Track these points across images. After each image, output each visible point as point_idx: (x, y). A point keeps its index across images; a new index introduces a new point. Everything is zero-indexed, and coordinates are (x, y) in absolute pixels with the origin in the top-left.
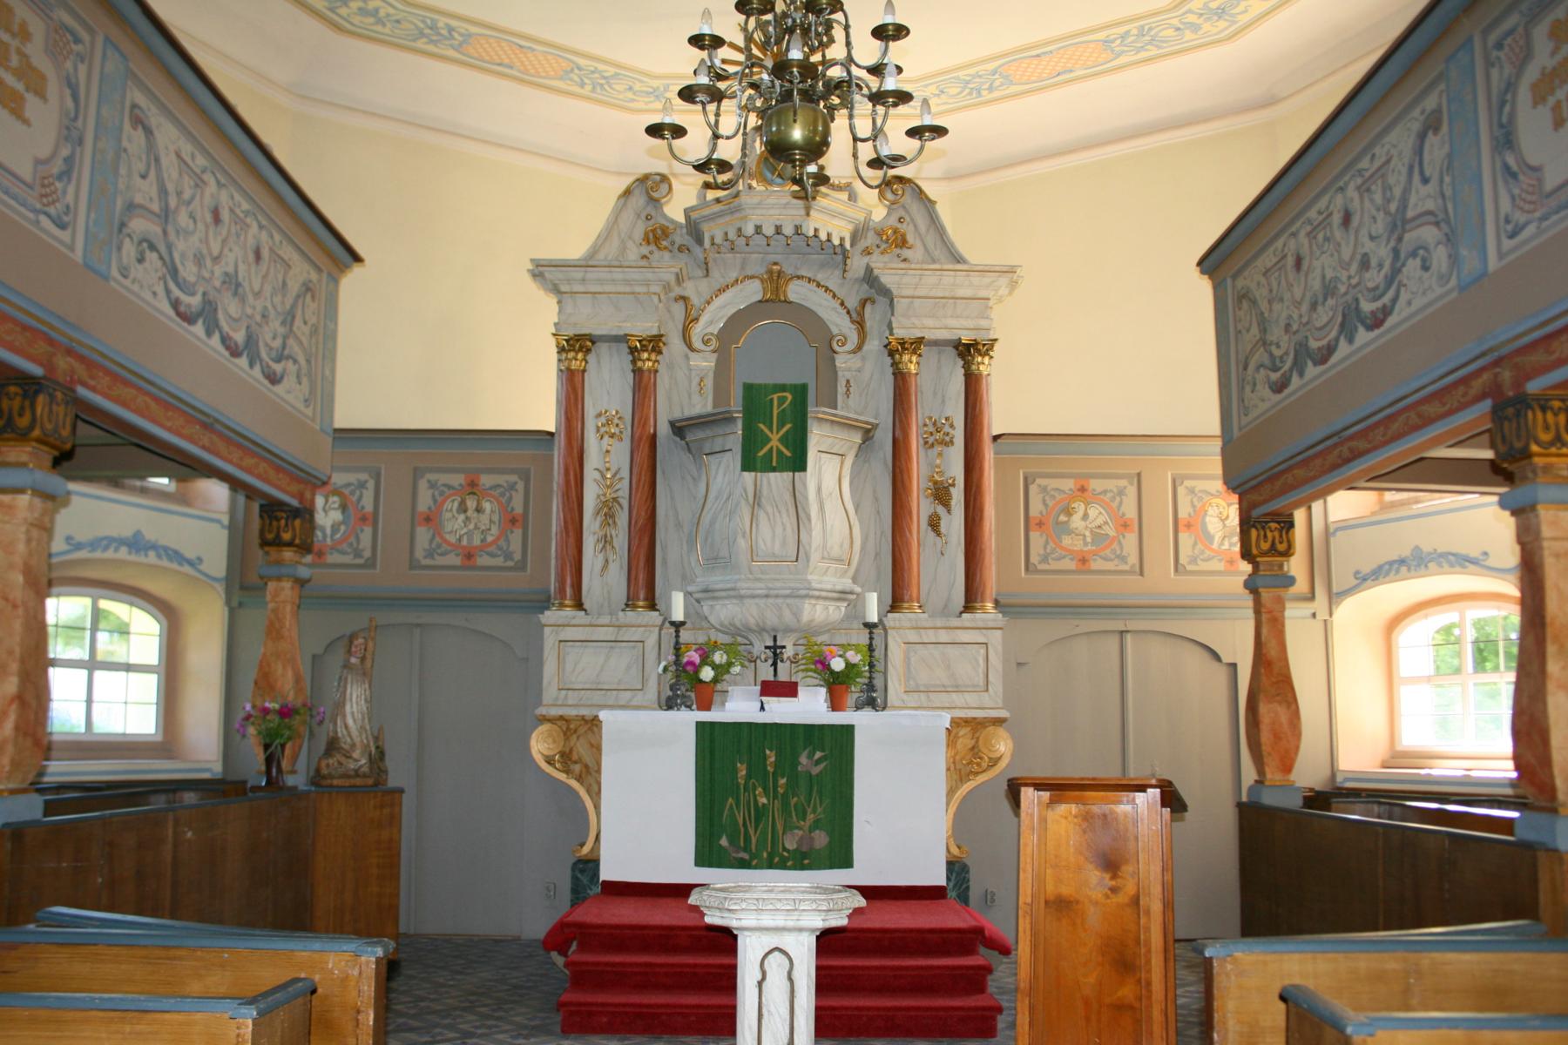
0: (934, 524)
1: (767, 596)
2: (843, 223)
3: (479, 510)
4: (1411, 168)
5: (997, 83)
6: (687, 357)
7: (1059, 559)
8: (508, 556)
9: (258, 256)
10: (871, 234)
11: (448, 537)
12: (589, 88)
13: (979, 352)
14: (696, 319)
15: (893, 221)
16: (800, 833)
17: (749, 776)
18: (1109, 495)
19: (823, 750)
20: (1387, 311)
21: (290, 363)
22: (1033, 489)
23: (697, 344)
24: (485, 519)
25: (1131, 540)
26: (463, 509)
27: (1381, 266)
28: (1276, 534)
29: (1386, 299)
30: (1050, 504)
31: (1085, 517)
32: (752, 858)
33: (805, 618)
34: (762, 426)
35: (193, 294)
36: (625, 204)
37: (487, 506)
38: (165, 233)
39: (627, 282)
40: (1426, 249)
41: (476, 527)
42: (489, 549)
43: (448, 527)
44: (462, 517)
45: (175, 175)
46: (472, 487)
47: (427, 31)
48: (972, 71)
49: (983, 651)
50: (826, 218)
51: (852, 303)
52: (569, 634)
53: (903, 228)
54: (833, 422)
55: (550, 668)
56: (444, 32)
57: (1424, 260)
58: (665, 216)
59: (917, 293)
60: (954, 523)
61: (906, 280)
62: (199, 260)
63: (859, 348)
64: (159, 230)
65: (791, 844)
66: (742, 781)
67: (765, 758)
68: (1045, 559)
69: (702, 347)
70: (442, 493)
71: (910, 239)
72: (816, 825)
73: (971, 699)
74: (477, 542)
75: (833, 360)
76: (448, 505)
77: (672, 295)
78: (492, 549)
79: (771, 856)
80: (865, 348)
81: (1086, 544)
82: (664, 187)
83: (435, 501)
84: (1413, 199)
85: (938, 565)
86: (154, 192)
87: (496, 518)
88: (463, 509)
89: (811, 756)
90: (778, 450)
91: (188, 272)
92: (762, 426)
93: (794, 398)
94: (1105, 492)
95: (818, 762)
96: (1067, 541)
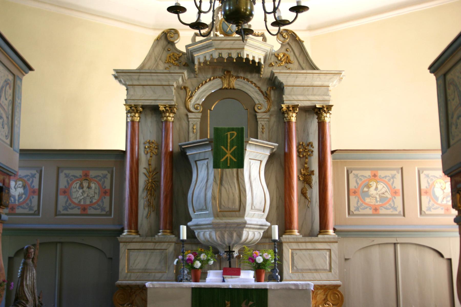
2: (260, 52)
3: (89, 187)
8: (103, 209)
11: (74, 200)
18: (387, 178)
19: (253, 301)
24: (92, 192)
26: (81, 187)
30: (360, 182)
31: (376, 189)
37: (93, 185)
41: (88, 196)
43: (74, 195)
44: (81, 191)
46: (86, 177)
70: (71, 180)
73: (323, 275)
75: (256, 116)
76: (74, 185)
78: (95, 206)
81: (377, 201)
87: (97, 191)
88: (81, 187)
90: (231, 159)
92: (222, 147)
94: (386, 177)
96: (368, 200)
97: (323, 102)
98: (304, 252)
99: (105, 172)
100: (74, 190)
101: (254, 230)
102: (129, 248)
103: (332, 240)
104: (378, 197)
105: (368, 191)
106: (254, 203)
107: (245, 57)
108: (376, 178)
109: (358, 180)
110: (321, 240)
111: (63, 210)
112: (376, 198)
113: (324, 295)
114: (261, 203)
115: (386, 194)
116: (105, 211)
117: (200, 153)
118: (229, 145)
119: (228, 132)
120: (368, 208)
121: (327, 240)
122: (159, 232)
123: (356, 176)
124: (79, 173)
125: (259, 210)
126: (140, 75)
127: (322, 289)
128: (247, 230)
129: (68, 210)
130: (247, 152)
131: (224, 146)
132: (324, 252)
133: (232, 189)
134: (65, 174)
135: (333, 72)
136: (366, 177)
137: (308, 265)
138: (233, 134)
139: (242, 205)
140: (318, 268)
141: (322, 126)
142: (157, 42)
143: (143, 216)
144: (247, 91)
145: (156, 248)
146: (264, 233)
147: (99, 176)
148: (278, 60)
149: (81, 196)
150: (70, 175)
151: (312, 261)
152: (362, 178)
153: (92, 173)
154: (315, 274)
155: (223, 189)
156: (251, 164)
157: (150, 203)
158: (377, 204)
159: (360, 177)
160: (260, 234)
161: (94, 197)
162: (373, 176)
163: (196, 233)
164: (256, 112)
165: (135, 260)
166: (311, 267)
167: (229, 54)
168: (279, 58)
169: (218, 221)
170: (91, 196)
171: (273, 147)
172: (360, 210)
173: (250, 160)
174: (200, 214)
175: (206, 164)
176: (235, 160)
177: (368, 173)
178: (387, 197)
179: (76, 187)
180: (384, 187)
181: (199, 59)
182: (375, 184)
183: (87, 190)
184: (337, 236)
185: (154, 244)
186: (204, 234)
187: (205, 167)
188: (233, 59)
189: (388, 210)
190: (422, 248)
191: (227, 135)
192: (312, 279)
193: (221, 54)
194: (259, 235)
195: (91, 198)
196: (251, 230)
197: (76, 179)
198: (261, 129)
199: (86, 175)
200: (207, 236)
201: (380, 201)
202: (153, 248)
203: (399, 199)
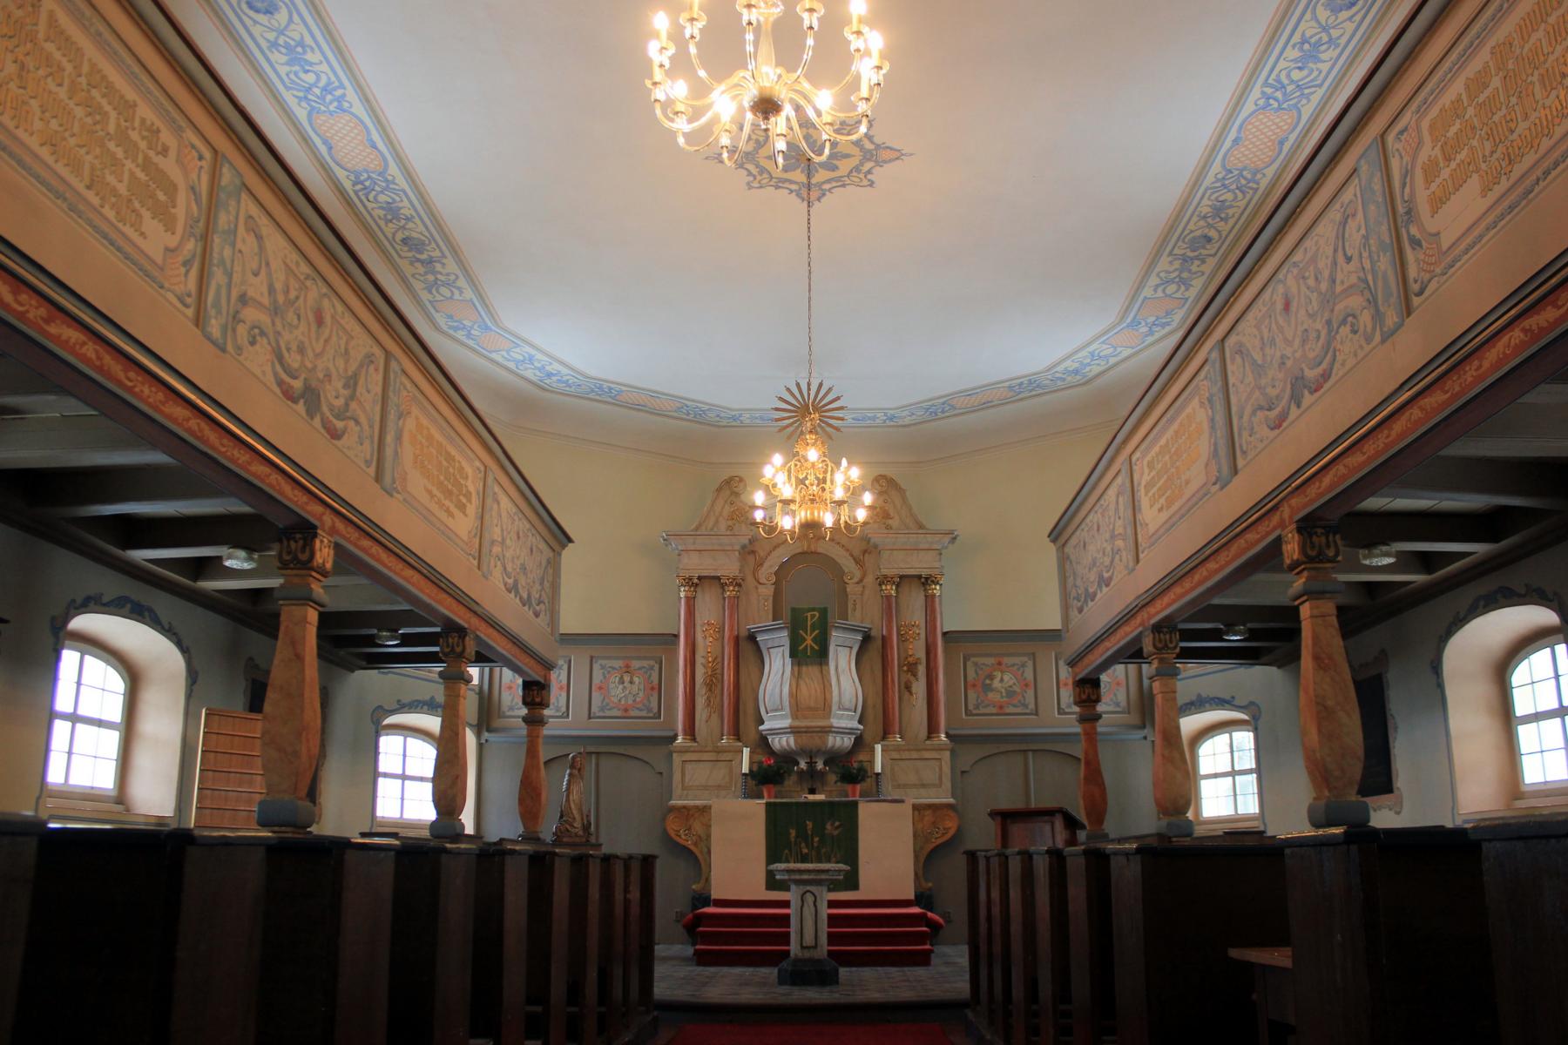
0: (908, 688)
4: (1335, 251)
8: (650, 710)
9: (320, 321)
20: (1326, 376)
21: (352, 423)
22: (969, 664)
23: (763, 580)
24: (635, 688)
25: (1030, 693)
26: (622, 681)
27: (1318, 338)
28: (1323, 539)
29: (1324, 365)
33: (830, 744)
35: (296, 378)
37: (636, 679)
38: (273, 324)
40: (1354, 316)
45: (282, 277)
46: (627, 669)
52: (688, 757)
55: (677, 777)
57: (1352, 325)
60: (919, 688)
62: (301, 350)
63: (861, 581)
64: (269, 321)
68: (977, 707)
84: (1339, 277)
85: (895, 755)
86: (265, 290)
88: (622, 681)
91: (294, 360)
96: (991, 695)
124: (618, 664)
141: (930, 600)
153: (636, 664)
155: (802, 683)
169: (797, 723)
177: (991, 661)
199: (627, 666)
203: (596, 681)
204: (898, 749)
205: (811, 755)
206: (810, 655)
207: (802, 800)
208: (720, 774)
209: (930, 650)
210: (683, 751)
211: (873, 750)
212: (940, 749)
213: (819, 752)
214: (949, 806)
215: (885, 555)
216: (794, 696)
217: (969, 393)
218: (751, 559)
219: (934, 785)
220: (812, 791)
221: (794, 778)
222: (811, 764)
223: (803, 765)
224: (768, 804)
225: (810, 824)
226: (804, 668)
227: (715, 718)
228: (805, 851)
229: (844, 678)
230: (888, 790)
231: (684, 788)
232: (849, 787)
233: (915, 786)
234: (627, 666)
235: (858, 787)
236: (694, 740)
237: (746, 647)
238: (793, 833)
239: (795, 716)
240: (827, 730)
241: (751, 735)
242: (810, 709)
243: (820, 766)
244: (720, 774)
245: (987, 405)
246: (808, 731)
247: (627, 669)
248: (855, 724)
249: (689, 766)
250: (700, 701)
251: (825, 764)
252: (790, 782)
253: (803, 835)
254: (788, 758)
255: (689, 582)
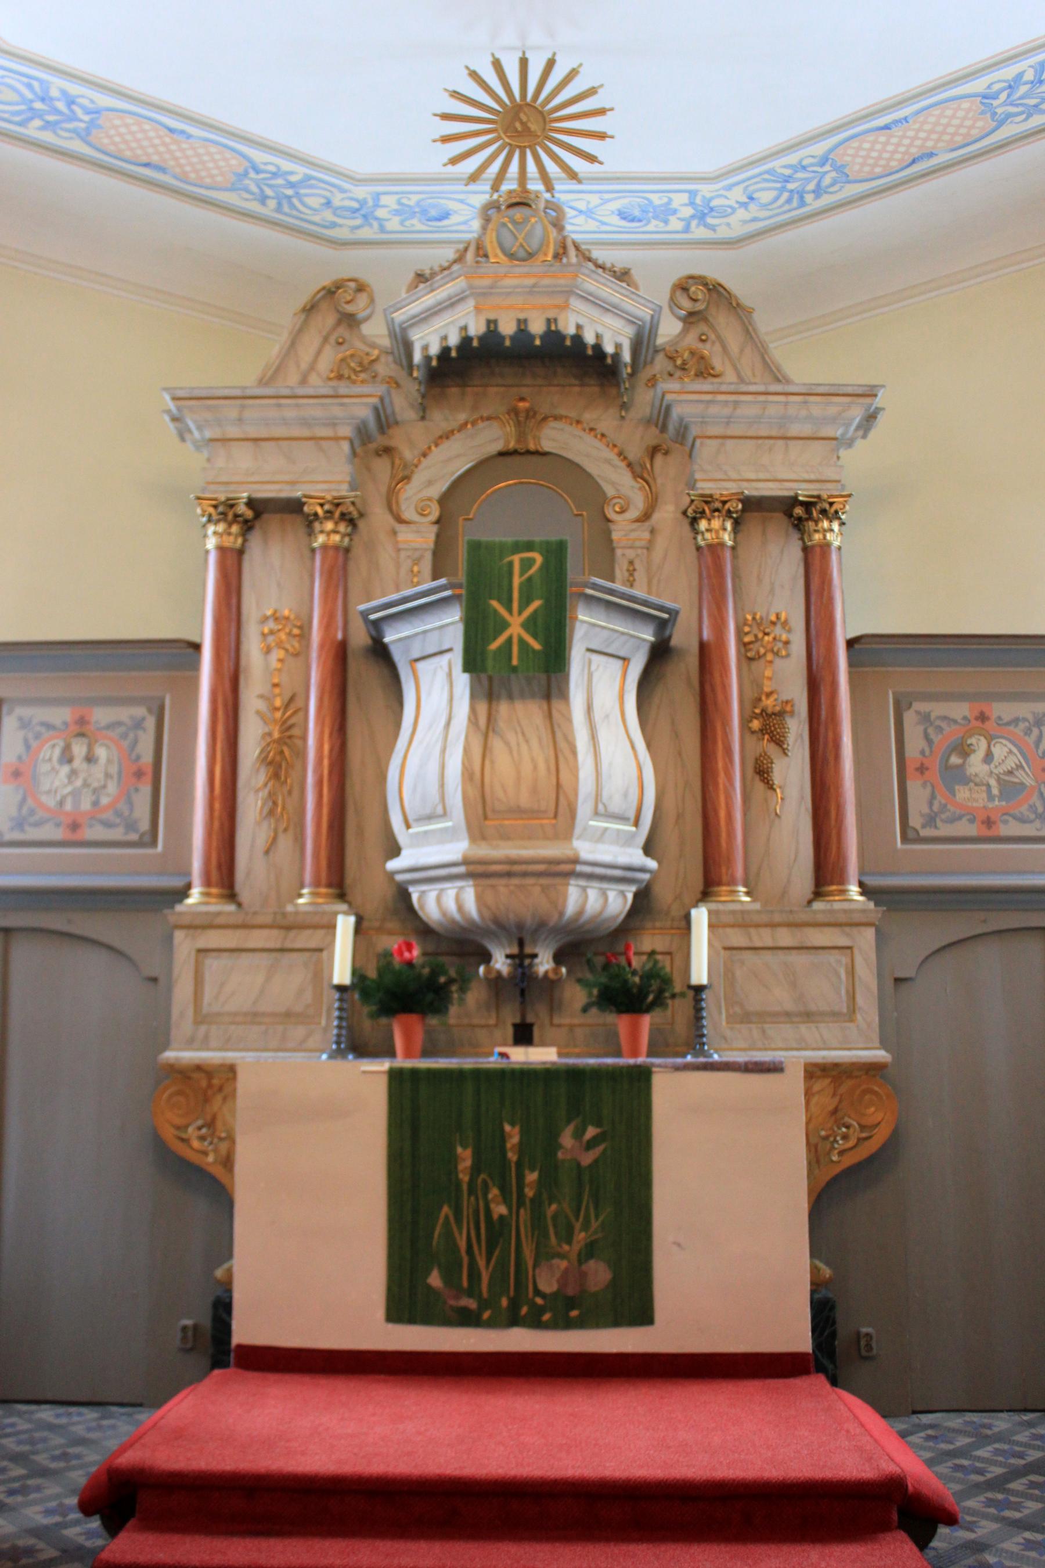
0: (762, 772)
1: (509, 875)
2: (617, 323)
3: (90, 759)
5: (827, 181)
6: (394, 533)
7: (952, 820)
8: (131, 826)
10: (660, 358)
11: (44, 798)
12: (272, 204)
13: (824, 512)
14: (407, 478)
15: (691, 340)
16: (564, 1264)
17: (476, 1169)
18: (1022, 725)
19: (598, 1124)
23: (409, 514)
24: (97, 772)
26: (67, 757)
30: (936, 738)
31: (989, 757)
32: (482, 1308)
33: (571, 907)
34: (495, 604)
36: (306, 322)
37: (101, 753)
39: (305, 422)
41: (86, 784)
42: (104, 816)
43: (46, 784)
44: (65, 770)
46: (82, 729)
47: (38, 105)
48: (793, 159)
49: (845, 960)
50: (594, 312)
51: (635, 452)
53: (706, 350)
54: (609, 604)
55: (183, 991)
56: (61, 106)
58: (363, 339)
59: (729, 433)
60: (793, 771)
61: (713, 410)
63: (646, 516)
65: (548, 1284)
66: (464, 1178)
67: (503, 1138)
69: (415, 517)
70: (38, 736)
71: (718, 363)
72: (590, 1251)
73: (829, 1031)
74: (86, 805)
75: (609, 532)
76: (45, 752)
77: (373, 446)
78: (108, 815)
79: (514, 1305)
80: (656, 516)
81: (991, 797)
82: (362, 299)
83: (28, 747)
85: (737, 938)
87: (114, 770)
89: (579, 1134)
90: (522, 642)
92: (495, 604)
93: (545, 566)
94: (1016, 721)
95: (590, 1145)
96: (962, 793)
97: (818, 486)
98: (767, 956)
99: (140, 711)
100: (45, 768)
101: (605, 885)
102: (201, 944)
103: (857, 918)
104: (993, 782)
105: (961, 767)
106: (605, 794)
107: (571, 331)
108: (988, 725)
109: (930, 730)
110: (820, 918)
111: (12, 829)
112: (988, 786)
113: (834, 1095)
114: (626, 795)
115: (1020, 773)
116: (136, 831)
117: (425, 632)
118: (516, 595)
119: (513, 553)
120: (964, 819)
121: (842, 918)
122: (300, 896)
123: (925, 718)
124: (61, 715)
125: (621, 818)
126: (243, 407)
127: (824, 1077)
128: (582, 883)
129: (27, 828)
130: (578, 624)
131: (499, 600)
132: (833, 957)
133: (530, 748)
134: (20, 719)
135: (850, 390)
136: (955, 722)
137: (781, 997)
138: (531, 562)
139: (562, 798)
140: (812, 1007)
141: (815, 564)
142: (303, 316)
143: (252, 846)
144: (577, 459)
145: (288, 945)
146: (636, 895)
147: (119, 724)
148: (676, 366)
149: (65, 786)
150: (35, 721)
151: (794, 985)
152: (944, 725)
153: (101, 716)
154: (803, 1028)
155: (496, 744)
156: (593, 668)
157: (275, 803)
158: (990, 805)
159: (938, 723)
160: (625, 897)
161: (104, 787)
162: (977, 719)
163: (415, 897)
164: (609, 521)
165: (222, 985)
166: (789, 1006)
167: (519, 321)
168: (679, 362)
169: (484, 851)
170: (95, 784)
171: (666, 616)
172: (939, 824)
173: (588, 654)
174: (426, 832)
175: (446, 669)
176: (537, 646)
177: (960, 710)
178: (1022, 784)
179: (50, 760)
180: (1011, 752)
181: (425, 348)
182: (983, 744)
183: (85, 765)
184: (871, 905)
185: (283, 932)
186: (438, 899)
187: (441, 677)
188: (532, 337)
189: (1027, 825)
190: (821, 951)
191: (511, 564)
192: (795, 1045)
193: (495, 322)
194: (620, 900)
195: (95, 791)
196: (596, 884)
197: (51, 733)
198: (626, 574)
199: (82, 721)
200: (451, 905)
201: (1001, 796)
202: (278, 946)
204: (743, 922)
205: (522, 938)
206: (518, 668)
207: (492, 1062)
208: (288, 985)
209: (818, 683)
210: (199, 925)
211: (686, 924)
212: (849, 923)
213: (541, 928)
214: (873, 1069)
215: (706, 450)
216: (475, 778)
217: (880, 119)
218: (382, 467)
219: (835, 1015)
220: (524, 1036)
221: (475, 995)
222: (521, 959)
223: (501, 963)
224: (396, 1077)
225: (513, 1135)
226: (503, 708)
227: (285, 843)
228: (500, 1210)
229: (608, 740)
230: (727, 1042)
231: (201, 1018)
232: (622, 1023)
233: (788, 1016)
234: (82, 721)
235: (646, 1021)
236: (231, 894)
237: (361, 670)
238: (465, 1157)
239: (477, 831)
240: (565, 870)
241: (373, 893)
242: (518, 812)
243: (544, 964)
244: (288, 985)
245: (920, 168)
246: (512, 871)
247: (82, 729)
248: (635, 856)
249: (213, 965)
250: (251, 805)
251: (559, 958)
252: (469, 1005)
253: (491, 1162)
254: (463, 945)
255: (225, 511)
